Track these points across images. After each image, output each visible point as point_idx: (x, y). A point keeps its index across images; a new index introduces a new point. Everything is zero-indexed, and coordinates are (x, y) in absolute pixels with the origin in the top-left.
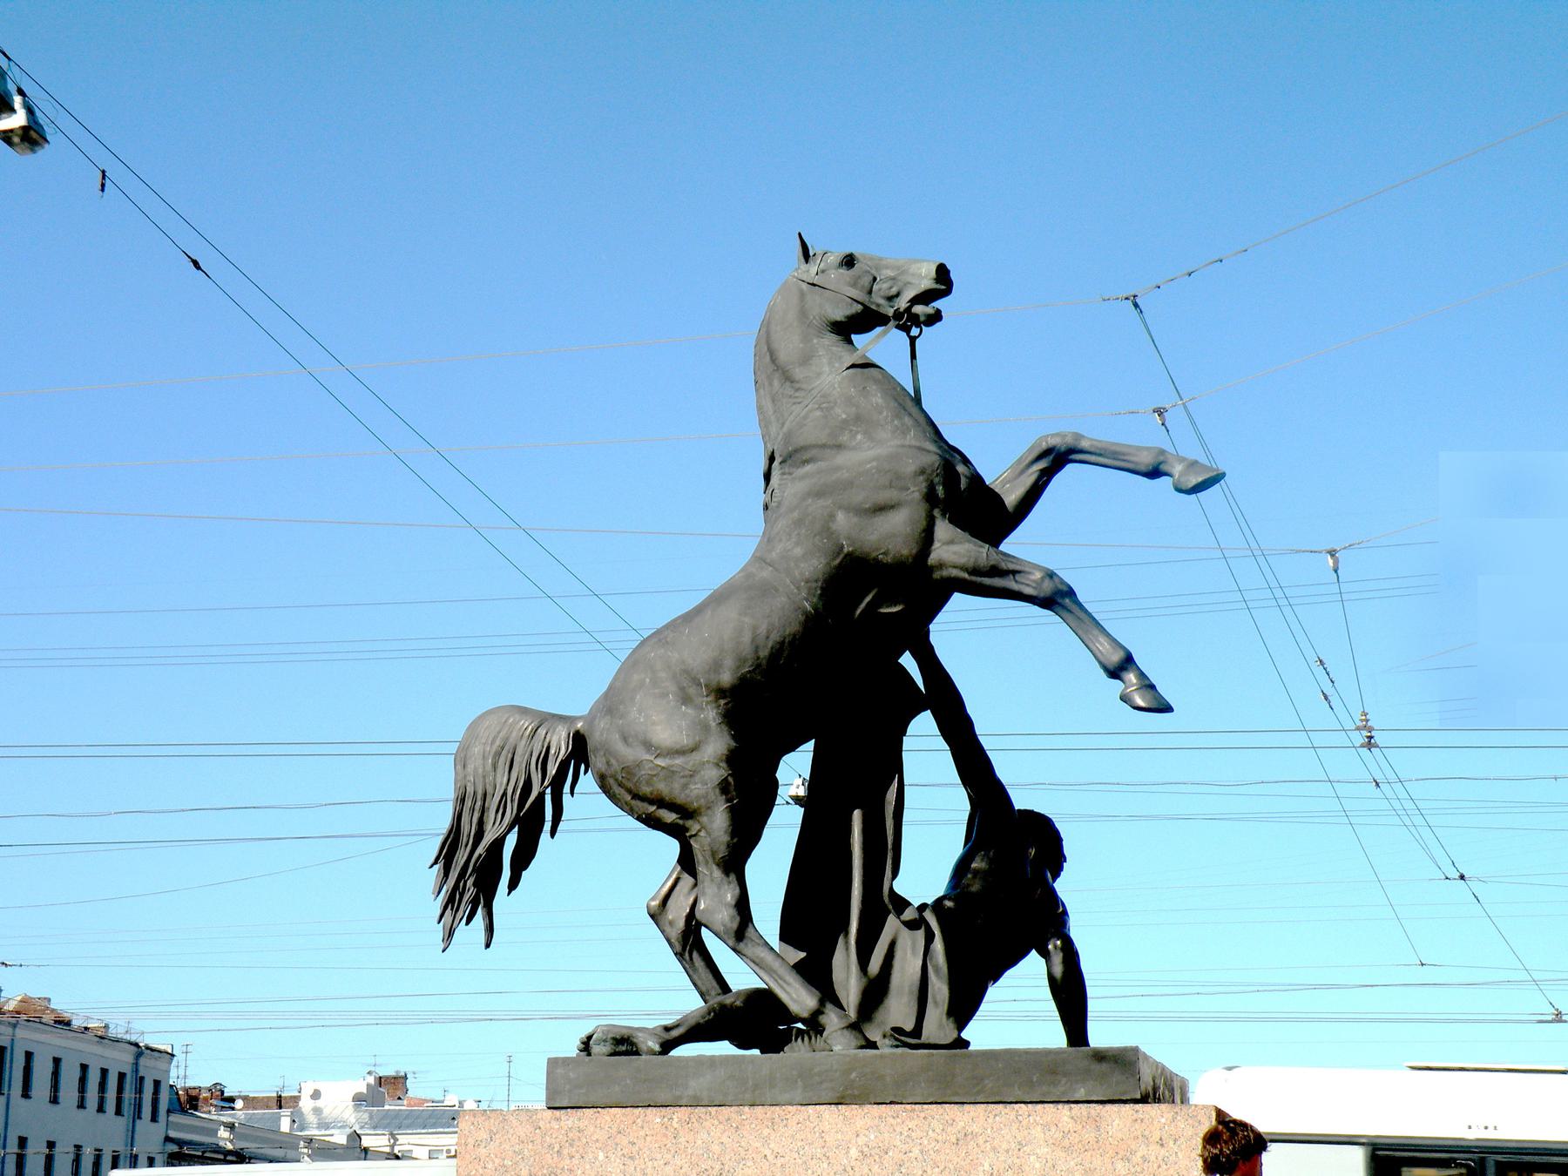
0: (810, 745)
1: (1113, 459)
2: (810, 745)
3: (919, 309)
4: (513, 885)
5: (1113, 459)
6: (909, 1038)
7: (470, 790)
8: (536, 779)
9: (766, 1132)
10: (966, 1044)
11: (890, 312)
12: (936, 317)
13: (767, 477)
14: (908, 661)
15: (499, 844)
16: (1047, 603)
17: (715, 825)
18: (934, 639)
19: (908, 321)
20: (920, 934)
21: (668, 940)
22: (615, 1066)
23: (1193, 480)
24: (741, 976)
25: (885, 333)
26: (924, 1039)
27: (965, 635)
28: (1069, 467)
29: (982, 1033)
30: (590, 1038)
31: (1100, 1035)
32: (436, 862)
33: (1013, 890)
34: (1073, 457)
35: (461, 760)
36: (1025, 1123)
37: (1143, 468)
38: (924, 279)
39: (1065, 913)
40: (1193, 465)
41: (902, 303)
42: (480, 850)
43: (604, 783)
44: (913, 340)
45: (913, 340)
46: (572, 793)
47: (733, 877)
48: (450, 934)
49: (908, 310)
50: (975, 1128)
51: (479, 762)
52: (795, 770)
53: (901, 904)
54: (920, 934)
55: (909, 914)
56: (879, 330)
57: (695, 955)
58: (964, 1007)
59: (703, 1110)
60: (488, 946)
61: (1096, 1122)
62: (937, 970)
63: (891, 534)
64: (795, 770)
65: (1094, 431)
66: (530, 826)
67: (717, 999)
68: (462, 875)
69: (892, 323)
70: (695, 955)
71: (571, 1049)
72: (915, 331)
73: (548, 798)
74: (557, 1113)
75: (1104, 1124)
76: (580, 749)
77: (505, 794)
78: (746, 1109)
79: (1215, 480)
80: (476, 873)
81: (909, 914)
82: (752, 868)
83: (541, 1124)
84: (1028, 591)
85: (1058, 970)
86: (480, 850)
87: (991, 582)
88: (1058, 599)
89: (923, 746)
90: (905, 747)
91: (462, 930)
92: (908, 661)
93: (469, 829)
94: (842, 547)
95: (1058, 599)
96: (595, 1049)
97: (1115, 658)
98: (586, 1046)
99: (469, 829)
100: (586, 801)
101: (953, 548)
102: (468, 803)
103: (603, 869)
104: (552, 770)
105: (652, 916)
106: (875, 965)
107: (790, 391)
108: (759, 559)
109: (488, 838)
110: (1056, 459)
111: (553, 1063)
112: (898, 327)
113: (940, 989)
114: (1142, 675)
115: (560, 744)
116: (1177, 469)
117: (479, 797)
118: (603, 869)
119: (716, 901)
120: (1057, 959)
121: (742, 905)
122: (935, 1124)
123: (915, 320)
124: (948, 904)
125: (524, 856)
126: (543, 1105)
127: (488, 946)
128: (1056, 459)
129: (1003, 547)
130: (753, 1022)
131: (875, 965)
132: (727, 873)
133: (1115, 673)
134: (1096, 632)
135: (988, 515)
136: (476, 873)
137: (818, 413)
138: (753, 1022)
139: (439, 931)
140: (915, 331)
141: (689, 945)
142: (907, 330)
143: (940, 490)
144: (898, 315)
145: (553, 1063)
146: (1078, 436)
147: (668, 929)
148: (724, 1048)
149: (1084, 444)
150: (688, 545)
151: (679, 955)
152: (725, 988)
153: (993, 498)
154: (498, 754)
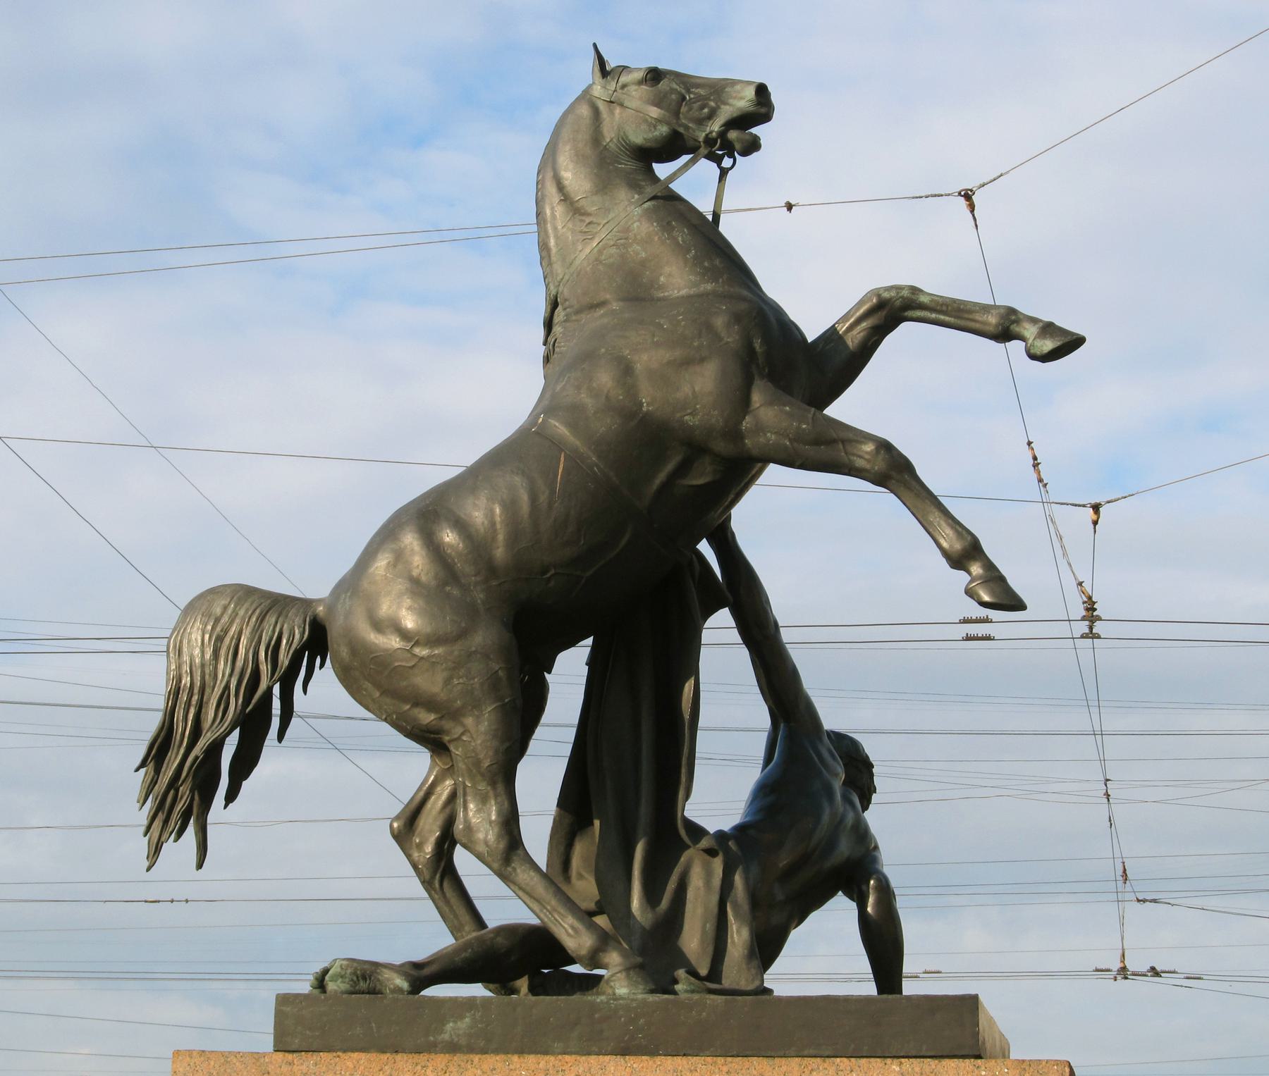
0: (590, 641)
1: (955, 315)
2: (590, 641)
3: (733, 135)
4: (231, 796)
5: (955, 315)
7: (186, 680)
8: (265, 669)
12: (753, 146)
13: (549, 325)
14: (704, 547)
15: (215, 749)
16: (880, 480)
17: (477, 732)
18: (735, 525)
21: (415, 866)
22: (347, 1004)
23: (1048, 345)
24: (502, 906)
25: (693, 162)
26: (727, 983)
27: (786, 525)
28: (905, 326)
30: (326, 971)
32: (143, 764)
33: (815, 824)
34: (909, 313)
37: (991, 329)
39: (876, 847)
40: (1048, 329)
41: (715, 127)
42: (198, 750)
43: (348, 678)
44: (724, 173)
45: (724, 173)
46: (305, 691)
47: (500, 787)
48: (155, 851)
49: (722, 134)
51: (197, 652)
52: (569, 674)
53: (696, 831)
56: (685, 158)
58: (767, 948)
60: (200, 865)
62: (736, 906)
63: (699, 390)
64: (569, 674)
65: (937, 282)
66: (254, 729)
67: (471, 934)
68: (174, 783)
70: (446, 884)
72: (727, 162)
73: (276, 690)
74: (290, 1056)
77: (227, 687)
82: (526, 771)
86: (198, 750)
87: (829, 452)
88: (894, 472)
90: (574, 730)
91: (169, 847)
92: (704, 547)
93: (182, 729)
95: (894, 472)
96: (331, 986)
99: (182, 729)
100: (323, 691)
101: (768, 414)
102: (184, 697)
103: (339, 777)
104: (284, 659)
108: (549, 405)
111: (284, 1001)
113: (739, 936)
114: (990, 566)
115: (295, 633)
116: (1030, 331)
117: (196, 691)
118: (339, 777)
119: (479, 818)
121: (510, 822)
123: (730, 150)
125: (246, 762)
126: (269, 1047)
127: (200, 865)
128: (890, 311)
130: (520, 961)
132: (493, 784)
133: (958, 561)
137: (613, 250)
139: (141, 845)
140: (727, 162)
141: (441, 875)
142: (718, 160)
143: (758, 344)
144: (710, 142)
145: (284, 1001)
146: (915, 290)
147: (416, 855)
148: (477, 990)
149: (924, 299)
152: (481, 923)
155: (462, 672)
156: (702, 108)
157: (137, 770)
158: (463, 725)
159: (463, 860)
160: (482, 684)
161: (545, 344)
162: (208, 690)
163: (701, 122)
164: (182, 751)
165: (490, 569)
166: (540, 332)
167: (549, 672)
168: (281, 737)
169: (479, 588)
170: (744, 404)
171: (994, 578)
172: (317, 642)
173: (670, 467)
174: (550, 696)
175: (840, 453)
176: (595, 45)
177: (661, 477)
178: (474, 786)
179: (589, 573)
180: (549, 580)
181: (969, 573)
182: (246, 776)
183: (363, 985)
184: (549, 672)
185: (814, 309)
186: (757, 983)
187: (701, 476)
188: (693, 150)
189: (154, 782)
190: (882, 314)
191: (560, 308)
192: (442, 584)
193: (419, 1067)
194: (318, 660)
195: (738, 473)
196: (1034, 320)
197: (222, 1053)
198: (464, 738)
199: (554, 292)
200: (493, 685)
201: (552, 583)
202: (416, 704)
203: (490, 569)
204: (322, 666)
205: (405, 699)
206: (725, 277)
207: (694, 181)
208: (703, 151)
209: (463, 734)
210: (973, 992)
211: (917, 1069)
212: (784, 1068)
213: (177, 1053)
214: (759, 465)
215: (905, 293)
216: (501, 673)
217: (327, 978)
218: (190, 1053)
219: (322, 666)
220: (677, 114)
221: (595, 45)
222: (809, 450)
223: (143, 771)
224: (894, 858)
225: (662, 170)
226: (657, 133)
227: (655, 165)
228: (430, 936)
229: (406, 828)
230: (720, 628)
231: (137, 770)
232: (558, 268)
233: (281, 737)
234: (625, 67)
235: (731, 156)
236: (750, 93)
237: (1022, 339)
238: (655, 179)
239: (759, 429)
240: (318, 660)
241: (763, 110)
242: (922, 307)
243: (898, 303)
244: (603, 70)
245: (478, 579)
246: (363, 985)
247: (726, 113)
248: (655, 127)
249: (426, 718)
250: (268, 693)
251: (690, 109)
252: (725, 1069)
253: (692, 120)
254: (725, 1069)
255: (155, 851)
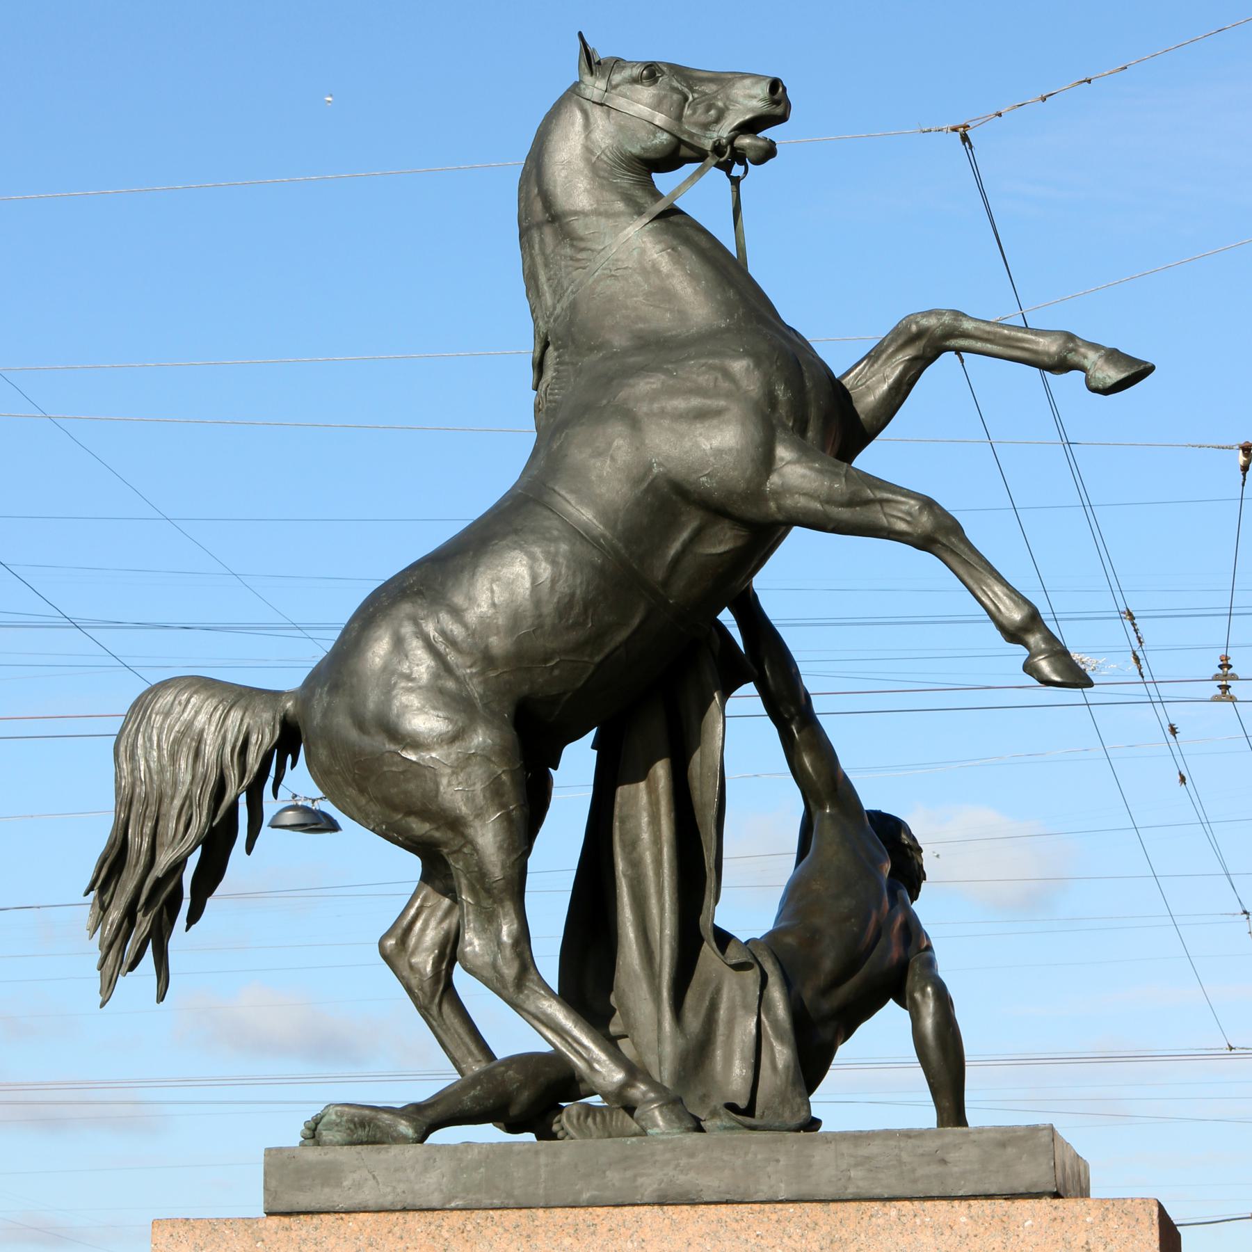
1: (1008, 347)
3: (745, 141)
4: (193, 917)
5: (1008, 347)
6: (744, 1111)
8: (233, 776)
9: (567, 1241)
10: (813, 1124)
11: (708, 145)
12: (769, 152)
13: (539, 366)
14: (726, 617)
15: (178, 866)
16: (925, 543)
19: (729, 157)
20: (752, 976)
23: (1113, 375)
24: (510, 1034)
25: (700, 173)
27: (802, 585)
29: (833, 1102)
30: (317, 1121)
31: (981, 1107)
32: (91, 889)
33: (862, 934)
35: (124, 748)
36: (908, 1225)
38: (749, 100)
40: (1114, 356)
41: (723, 131)
44: (736, 182)
45: (736, 182)
48: (108, 986)
49: (731, 141)
50: (844, 1233)
52: (577, 765)
53: (723, 939)
54: (752, 976)
55: (734, 955)
57: (446, 1008)
58: (812, 1065)
59: (482, 1214)
60: (161, 997)
61: (1004, 1219)
63: (712, 444)
64: (577, 765)
65: (986, 305)
67: (476, 1067)
69: (711, 160)
71: (292, 1137)
72: (737, 170)
73: (243, 799)
75: (1012, 1227)
76: (290, 739)
78: (541, 1212)
79: (1152, 368)
80: (149, 897)
81: (734, 955)
83: (264, 1234)
84: (902, 526)
85: (929, 1023)
87: (859, 514)
88: (940, 536)
89: (742, 728)
92: (726, 617)
93: (139, 843)
94: (650, 468)
95: (940, 536)
96: (326, 1135)
97: (1016, 615)
98: (313, 1133)
101: (795, 473)
102: (137, 808)
103: (319, 904)
105: (386, 957)
106: (693, 1022)
107: (568, 251)
109: (164, 860)
110: (925, 344)
112: (718, 165)
113: (781, 1054)
114: (1050, 638)
116: (1091, 358)
118: (319, 904)
120: (929, 1008)
121: (523, 937)
122: (791, 1229)
123: (739, 156)
124: (789, 940)
127: (161, 997)
128: (925, 344)
129: (854, 464)
130: (534, 1099)
131: (693, 1022)
133: (1013, 635)
134: (991, 581)
135: (838, 421)
136: (149, 897)
138: (534, 1099)
139: (94, 980)
140: (737, 170)
141: (437, 998)
142: (726, 167)
144: (718, 149)
146: (958, 314)
148: (489, 1133)
149: (968, 325)
150: (382, 451)
151: (424, 1010)
153: (838, 394)
154: (177, 742)
155: (462, 776)
156: (708, 110)
157: (87, 894)
158: (463, 835)
159: (460, 977)
160: (484, 790)
161: (536, 388)
162: (166, 801)
163: (706, 126)
164: (140, 869)
165: (487, 659)
166: (529, 374)
167: (556, 768)
168: (249, 848)
169: (475, 681)
170: (767, 462)
171: (1059, 653)
172: (290, 739)
173: (685, 535)
174: (554, 791)
175: (878, 516)
176: (580, 34)
177: (675, 548)
178: (478, 903)
179: (598, 659)
180: (553, 668)
181: (1026, 645)
182: (210, 892)
183: (362, 1134)
184: (556, 768)
185: (842, 342)
186: (804, 1113)
187: (722, 542)
188: (700, 156)
189: (104, 908)
190: (921, 344)
191: (551, 348)
192: (436, 676)
193: (433, 1227)
194: (289, 758)
195: (762, 537)
196: (1095, 347)
197: (210, 1221)
198: (465, 850)
199: (543, 329)
200: (495, 790)
201: (556, 672)
202: (410, 812)
203: (487, 659)
204: (293, 765)
205: (395, 808)
206: (741, 311)
207: (701, 194)
208: (711, 160)
209: (464, 846)
210: (1047, 1122)
211: (988, 1212)
212: (841, 1215)
213: (157, 1223)
214: (783, 528)
215: (947, 319)
216: (504, 777)
217: (320, 1127)
218: (173, 1222)
219: (293, 765)
220: (679, 117)
221: (580, 34)
222: (844, 514)
223: (93, 894)
224: (951, 962)
225: (664, 182)
226: (657, 141)
227: (654, 175)
228: (428, 1072)
229: (395, 948)
230: (746, 702)
231: (87, 894)
232: (548, 299)
233: (249, 848)
234: (618, 60)
235: (742, 162)
236: (762, 90)
237: (1082, 369)
238: (657, 195)
239: (786, 490)
240: (289, 758)
241: (779, 110)
242: (966, 335)
243: (939, 332)
244: (590, 62)
245: (474, 670)
246: (362, 1134)
247: (733, 120)
248: (654, 134)
249: (420, 828)
250: (234, 806)
251: (694, 112)
252: (774, 1217)
253: (696, 124)
254: (774, 1217)
255: (108, 986)
